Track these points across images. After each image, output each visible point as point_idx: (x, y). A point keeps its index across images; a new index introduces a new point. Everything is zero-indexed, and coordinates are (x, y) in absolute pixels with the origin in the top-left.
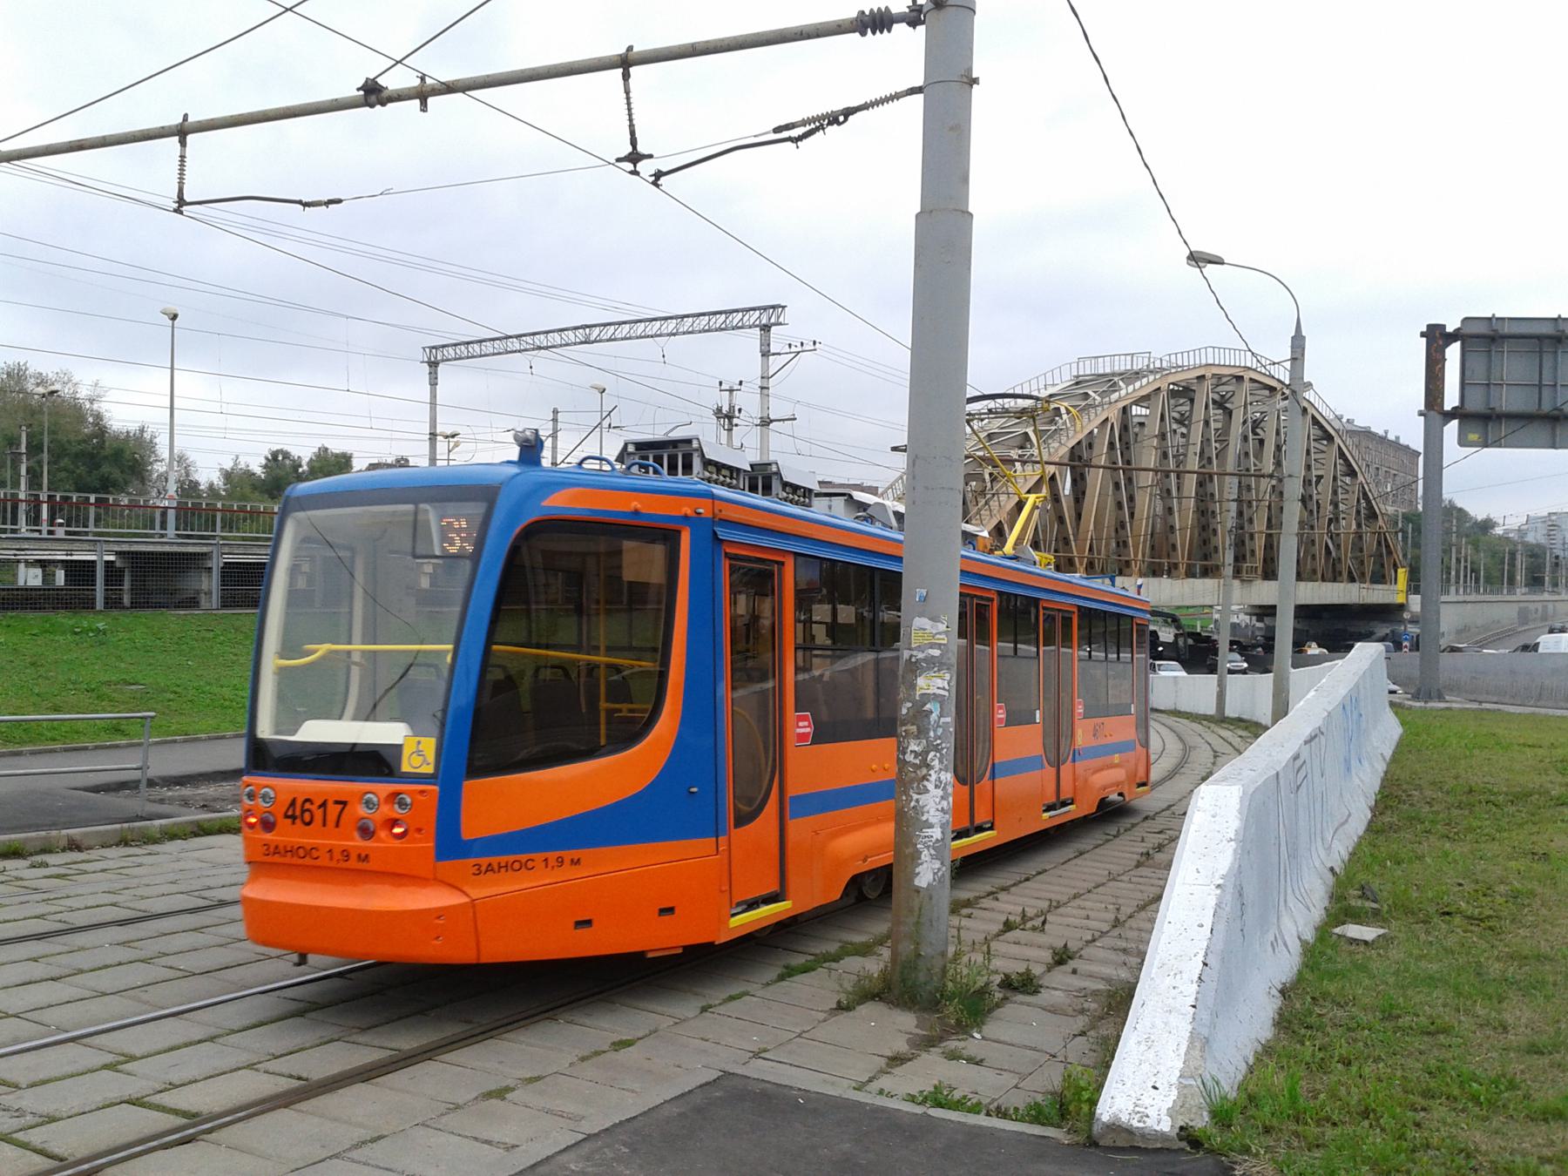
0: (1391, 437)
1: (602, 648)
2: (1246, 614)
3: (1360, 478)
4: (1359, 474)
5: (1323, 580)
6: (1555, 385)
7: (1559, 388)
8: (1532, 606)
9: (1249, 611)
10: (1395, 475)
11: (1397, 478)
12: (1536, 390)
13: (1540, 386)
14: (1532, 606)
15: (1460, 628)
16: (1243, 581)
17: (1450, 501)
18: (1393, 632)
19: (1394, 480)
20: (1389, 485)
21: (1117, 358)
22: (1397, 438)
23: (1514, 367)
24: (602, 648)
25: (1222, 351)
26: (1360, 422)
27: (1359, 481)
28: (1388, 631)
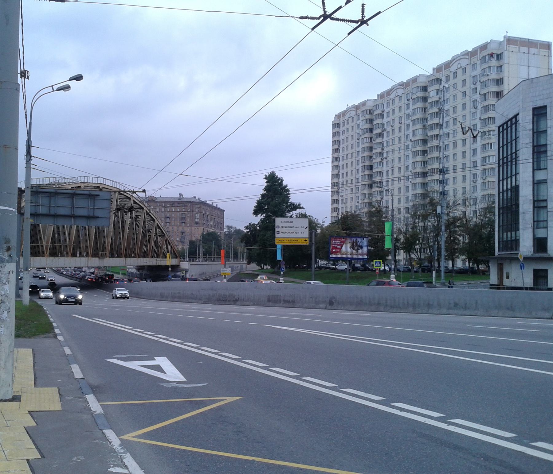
0: (214, 205)
1: (121, 274)
2: (135, 269)
3: (157, 222)
4: (156, 220)
5: (139, 257)
6: (55, 206)
7: (56, 207)
8: (235, 265)
9: (136, 268)
10: (214, 218)
11: (215, 219)
12: (49, 208)
13: (50, 206)
14: (235, 265)
15: (201, 273)
16: (99, 258)
17: (235, 228)
18: (175, 275)
19: (214, 220)
20: (212, 222)
21: (38, 179)
22: (217, 205)
23: (43, 201)
24: (121, 274)
25: (89, 178)
26: (203, 199)
27: (156, 223)
28: (173, 275)
